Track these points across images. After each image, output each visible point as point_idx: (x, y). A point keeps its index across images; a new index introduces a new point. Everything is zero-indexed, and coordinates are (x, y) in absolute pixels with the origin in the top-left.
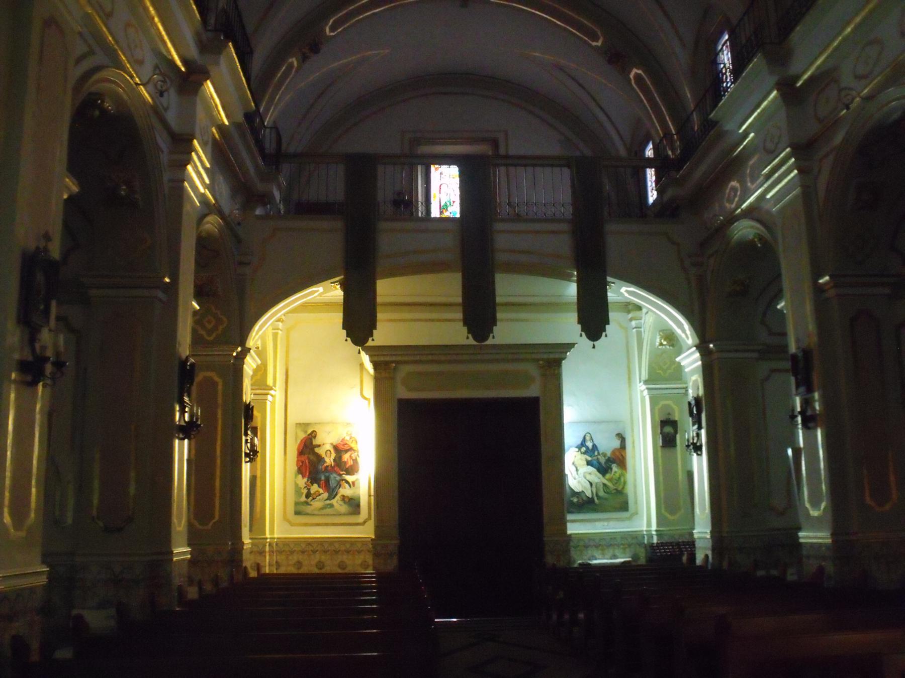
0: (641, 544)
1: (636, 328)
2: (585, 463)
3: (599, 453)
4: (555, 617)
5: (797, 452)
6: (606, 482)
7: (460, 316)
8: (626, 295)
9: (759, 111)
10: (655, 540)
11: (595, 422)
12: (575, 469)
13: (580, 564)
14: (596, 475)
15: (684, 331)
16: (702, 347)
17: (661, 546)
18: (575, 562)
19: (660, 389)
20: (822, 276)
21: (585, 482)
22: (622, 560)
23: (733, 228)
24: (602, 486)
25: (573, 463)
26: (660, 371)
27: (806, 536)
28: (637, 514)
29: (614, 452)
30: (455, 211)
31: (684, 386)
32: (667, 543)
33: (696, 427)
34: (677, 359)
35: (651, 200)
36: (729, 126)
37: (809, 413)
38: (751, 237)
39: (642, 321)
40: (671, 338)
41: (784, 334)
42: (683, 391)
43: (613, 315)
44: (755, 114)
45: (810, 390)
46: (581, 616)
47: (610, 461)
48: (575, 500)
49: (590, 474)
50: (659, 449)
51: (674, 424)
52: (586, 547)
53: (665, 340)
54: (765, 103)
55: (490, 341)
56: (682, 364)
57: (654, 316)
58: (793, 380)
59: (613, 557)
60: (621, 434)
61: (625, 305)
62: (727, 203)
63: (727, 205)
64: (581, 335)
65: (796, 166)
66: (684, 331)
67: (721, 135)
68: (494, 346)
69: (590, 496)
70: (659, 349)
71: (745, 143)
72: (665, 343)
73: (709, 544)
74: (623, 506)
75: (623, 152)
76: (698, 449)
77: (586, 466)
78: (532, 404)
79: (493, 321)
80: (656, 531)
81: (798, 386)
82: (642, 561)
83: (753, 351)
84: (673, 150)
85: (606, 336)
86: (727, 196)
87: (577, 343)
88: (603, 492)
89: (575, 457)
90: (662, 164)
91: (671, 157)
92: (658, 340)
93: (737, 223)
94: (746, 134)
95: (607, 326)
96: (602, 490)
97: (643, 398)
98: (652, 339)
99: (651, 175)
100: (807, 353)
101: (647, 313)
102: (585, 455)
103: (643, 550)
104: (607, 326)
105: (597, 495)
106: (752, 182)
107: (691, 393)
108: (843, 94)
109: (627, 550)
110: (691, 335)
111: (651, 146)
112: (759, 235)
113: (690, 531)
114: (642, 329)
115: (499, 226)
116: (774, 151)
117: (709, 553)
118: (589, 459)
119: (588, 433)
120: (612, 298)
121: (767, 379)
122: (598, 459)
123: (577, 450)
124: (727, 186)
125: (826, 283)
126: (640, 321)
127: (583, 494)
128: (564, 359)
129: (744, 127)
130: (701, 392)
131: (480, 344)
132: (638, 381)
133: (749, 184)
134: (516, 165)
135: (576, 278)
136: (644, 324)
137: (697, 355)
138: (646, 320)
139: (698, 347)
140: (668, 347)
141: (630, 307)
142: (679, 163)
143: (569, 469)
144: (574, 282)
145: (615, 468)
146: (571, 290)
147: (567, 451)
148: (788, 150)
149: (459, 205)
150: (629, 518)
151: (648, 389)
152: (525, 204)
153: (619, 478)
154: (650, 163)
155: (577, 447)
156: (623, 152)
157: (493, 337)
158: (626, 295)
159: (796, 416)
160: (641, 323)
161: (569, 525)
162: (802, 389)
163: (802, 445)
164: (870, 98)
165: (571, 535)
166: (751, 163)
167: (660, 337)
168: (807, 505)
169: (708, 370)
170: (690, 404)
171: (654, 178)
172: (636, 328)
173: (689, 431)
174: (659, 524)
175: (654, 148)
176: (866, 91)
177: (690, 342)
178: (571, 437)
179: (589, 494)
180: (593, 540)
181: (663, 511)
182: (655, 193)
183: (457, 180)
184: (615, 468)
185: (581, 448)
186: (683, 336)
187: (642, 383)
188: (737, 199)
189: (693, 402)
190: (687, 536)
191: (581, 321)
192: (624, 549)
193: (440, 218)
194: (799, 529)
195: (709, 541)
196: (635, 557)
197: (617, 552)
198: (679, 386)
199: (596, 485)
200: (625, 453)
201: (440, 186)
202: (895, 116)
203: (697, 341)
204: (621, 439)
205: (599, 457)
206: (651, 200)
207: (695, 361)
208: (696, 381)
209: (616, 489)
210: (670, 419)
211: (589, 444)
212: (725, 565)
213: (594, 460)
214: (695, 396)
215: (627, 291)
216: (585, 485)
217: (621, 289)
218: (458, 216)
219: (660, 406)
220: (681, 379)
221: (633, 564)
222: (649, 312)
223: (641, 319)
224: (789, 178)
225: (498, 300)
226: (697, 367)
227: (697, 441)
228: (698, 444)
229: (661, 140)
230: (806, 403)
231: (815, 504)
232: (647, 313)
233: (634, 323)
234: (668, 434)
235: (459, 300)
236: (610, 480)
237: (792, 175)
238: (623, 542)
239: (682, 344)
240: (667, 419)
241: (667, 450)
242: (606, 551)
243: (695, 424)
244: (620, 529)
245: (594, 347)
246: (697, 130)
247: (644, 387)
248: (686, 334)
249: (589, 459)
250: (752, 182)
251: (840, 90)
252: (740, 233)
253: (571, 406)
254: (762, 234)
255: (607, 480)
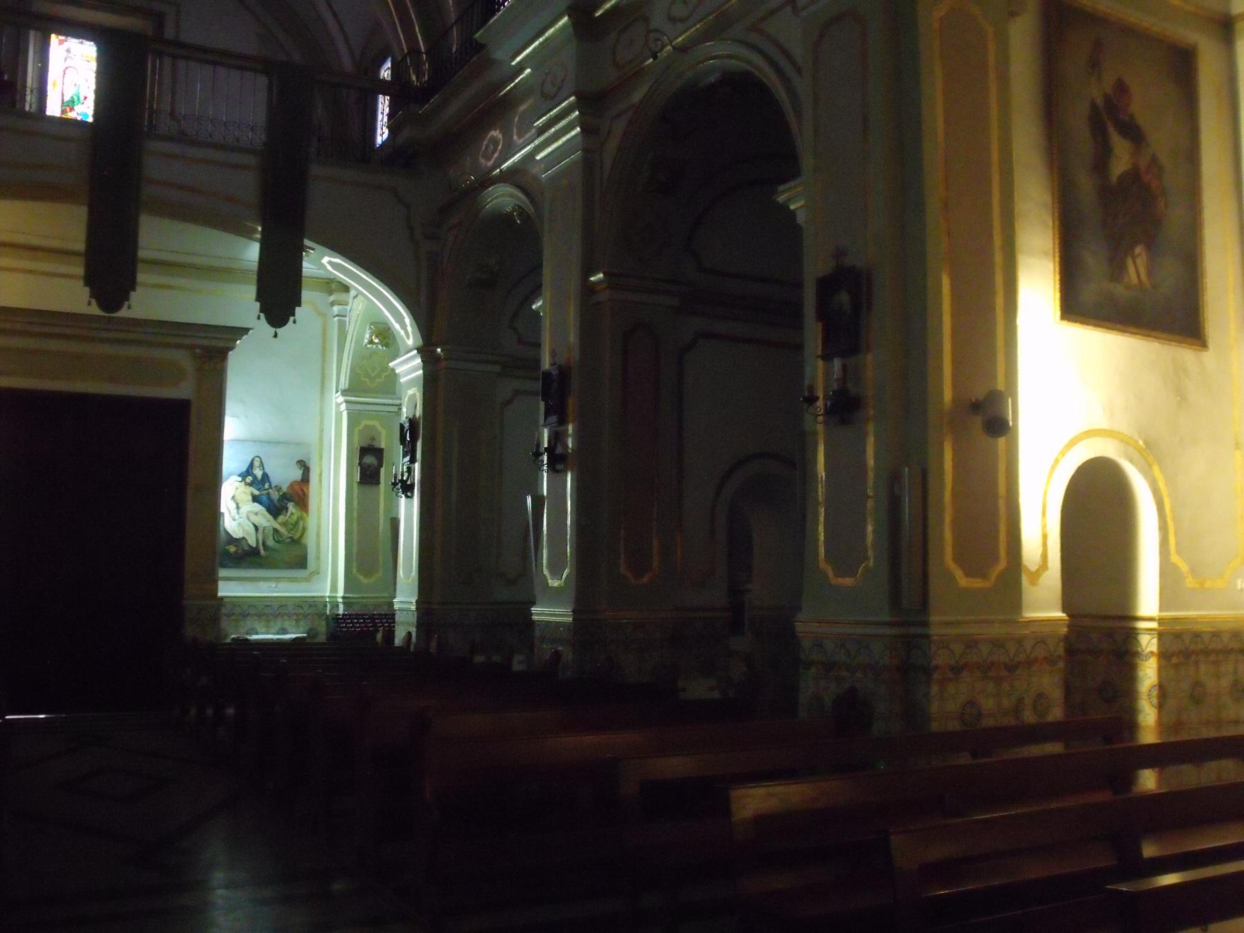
0: (321, 615)
1: (337, 315)
2: (250, 498)
3: (270, 486)
4: (193, 711)
5: (539, 502)
6: (277, 526)
7: (80, 271)
8: (329, 268)
9: (541, 40)
10: (341, 611)
11: (269, 442)
12: (235, 506)
13: (233, 639)
14: (265, 517)
15: (404, 326)
16: (425, 351)
17: (356, 619)
18: (226, 636)
19: (365, 403)
20: (594, 273)
21: (248, 525)
22: (294, 636)
23: (487, 193)
24: (272, 532)
25: (233, 498)
26: (366, 379)
27: (541, 613)
28: (318, 573)
29: (292, 486)
30: (85, 111)
31: (397, 402)
32: (357, 615)
33: (408, 458)
34: (391, 365)
35: (379, 140)
36: (498, 55)
37: (559, 450)
38: (509, 209)
39: (348, 308)
40: (385, 335)
41: (538, 345)
42: (395, 409)
43: (306, 295)
44: (537, 43)
45: (562, 421)
46: (230, 711)
47: (285, 498)
48: (232, 549)
49: (256, 514)
50: (355, 485)
51: (378, 453)
52: (245, 615)
53: (377, 337)
54: (551, 31)
55: (123, 313)
56: (397, 372)
57: (366, 301)
58: (542, 405)
59: (281, 632)
60: (304, 462)
61: (327, 283)
62: (483, 158)
63: (482, 161)
64: (259, 318)
65: (581, 122)
66: (404, 326)
67: (489, 63)
68: (136, 323)
69: (254, 545)
70: (368, 348)
71: (517, 81)
72: (377, 341)
73: (413, 619)
74: (301, 562)
75: (347, 64)
76: (407, 489)
77: (251, 503)
78: (182, 407)
79: (132, 285)
80: (343, 598)
81: (548, 413)
82: (322, 638)
83: (495, 363)
84: (419, 74)
85: (294, 322)
86: (484, 148)
87: (252, 329)
88: (273, 541)
89: (237, 488)
90: (399, 91)
91: (415, 84)
92: (367, 336)
93: (492, 187)
94: (520, 68)
95: (297, 308)
96: (272, 538)
97: (339, 414)
98: (358, 333)
99: (383, 105)
100: (564, 373)
101: (355, 297)
102: (251, 488)
103: (324, 623)
104: (297, 308)
105: (264, 543)
106: (520, 136)
107: (405, 413)
108: (652, 36)
109: (302, 623)
110: (413, 333)
111: (388, 64)
112: (520, 207)
113: (389, 600)
114: (347, 319)
115: (154, 145)
116: (555, 96)
117: (413, 630)
118: (257, 493)
119: (258, 457)
120: (307, 270)
121: (509, 402)
122: (268, 494)
123: (240, 479)
124: (486, 136)
125: (599, 282)
126: (345, 307)
127: (244, 543)
128: (232, 349)
129: (518, 59)
130: (419, 412)
131: (107, 315)
132: (334, 390)
133: (515, 137)
134: (187, 58)
135: (259, 236)
136: (350, 312)
137: (419, 361)
138: (354, 307)
139: (420, 350)
140: (380, 347)
141: (333, 286)
142: (424, 94)
143: (226, 505)
144: (257, 241)
145: (291, 506)
146: (252, 252)
147: (225, 481)
148: (572, 98)
149: (48, 94)
150: (308, 580)
151: (347, 402)
152: (237, 125)
153: (297, 523)
154: (385, 88)
155: (239, 476)
156: (347, 64)
157: (129, 307)
158: (329, 268)
159: (542, 454)
160: (346, 309)
161: (221, 584)
162: (553, 419)
163: (545, 494)
164: (682, 50)
165: (222, 598)
166: (523, 107)
167: (371, 333)
168: (546, 572)
169: (431, 383)
170: (402, 426)
171: (387, 110)
172: (337, 315)
173: (397, 462)
174: (347, 588)
175: (393, 68)
176: (680, 39)
177: (410, 342)
178: (232, 460)
179: (252, 542)
180: (254, 606)
181: (355, 570)
182: (386, 131)
183: (93, 66)
184: (291, 506)
185: (246, 477)
186: (402, 333)
187: (339, 393)
188: (496, 155)
189: (407, 425)
190: (386, 607)
191: (259, 297)
192: (297, 621)
193: (59, 118)
194: (533, 603)
195: (414, 615)
196: (312, 633)
197: (287, 624)
198: (390, 401)
199: (264, 530)
200: (308, 489)
201: (67, 68)
202: (712, 79)
203: (420, 342)
204: (303, 468)
205: (270, 490)
206: (379, 140)
207: (415, 369)
208: (414, 395)
209: (291, 538)
210: (373, 446)
211: (258, 473)
212: (434, 644)
213: (263, 495)
214: (411, 416)
215: (330, 263)
216: (247, 528)
217: (322, 258)
218: (90, 120)
219: (361, 427)
220: (395, 393)
221: (308, 641)
222: (359, 296)
223: (346, 305)
224: (568, 136)
225: (142, 254)
226: (417, 377)
227: (408, 478)
228: (409, 483)
229: (404, 58)
230: (557, 438)
231: (556, 570)
232: (355, 297)
233: (336, 309)
234: (369, 466)
235: (80, 246)
236: (284, 524)
237: (573, 133)
238: (296, 611)
239: (400, 344)
240: (369, 445)
241: (367, 489)
242: (272, 623)
243: (407, 455)
244: (294, 592)
245: (276, 336)
246: (455, 52)
247: (341, 399)
248: (407, 331)
249: (257, 493)
250: (520, 136)
251: (649, 31)
252: (494, 202)
253: (237, 417)
254: (522, 206)
255: (280, 524)
